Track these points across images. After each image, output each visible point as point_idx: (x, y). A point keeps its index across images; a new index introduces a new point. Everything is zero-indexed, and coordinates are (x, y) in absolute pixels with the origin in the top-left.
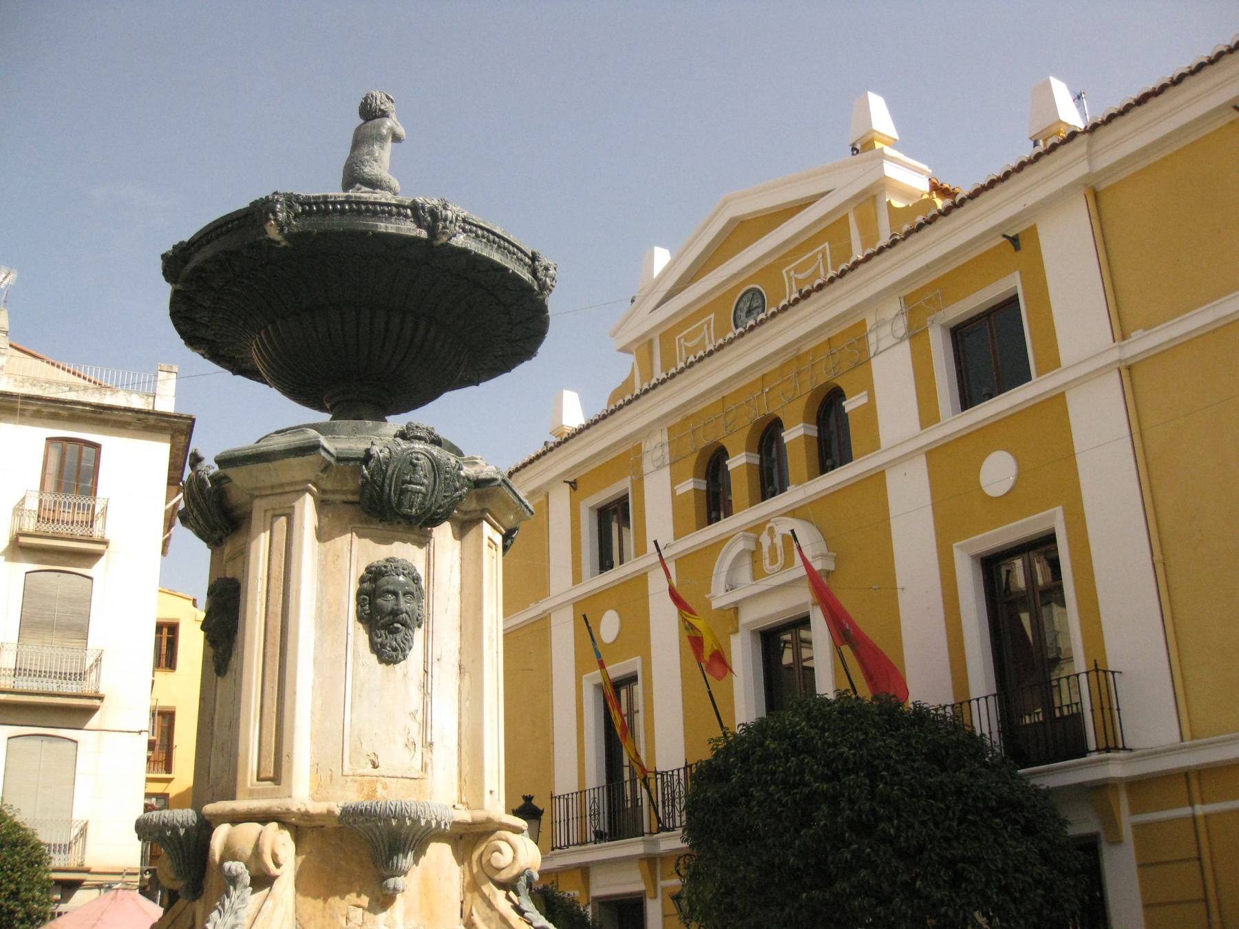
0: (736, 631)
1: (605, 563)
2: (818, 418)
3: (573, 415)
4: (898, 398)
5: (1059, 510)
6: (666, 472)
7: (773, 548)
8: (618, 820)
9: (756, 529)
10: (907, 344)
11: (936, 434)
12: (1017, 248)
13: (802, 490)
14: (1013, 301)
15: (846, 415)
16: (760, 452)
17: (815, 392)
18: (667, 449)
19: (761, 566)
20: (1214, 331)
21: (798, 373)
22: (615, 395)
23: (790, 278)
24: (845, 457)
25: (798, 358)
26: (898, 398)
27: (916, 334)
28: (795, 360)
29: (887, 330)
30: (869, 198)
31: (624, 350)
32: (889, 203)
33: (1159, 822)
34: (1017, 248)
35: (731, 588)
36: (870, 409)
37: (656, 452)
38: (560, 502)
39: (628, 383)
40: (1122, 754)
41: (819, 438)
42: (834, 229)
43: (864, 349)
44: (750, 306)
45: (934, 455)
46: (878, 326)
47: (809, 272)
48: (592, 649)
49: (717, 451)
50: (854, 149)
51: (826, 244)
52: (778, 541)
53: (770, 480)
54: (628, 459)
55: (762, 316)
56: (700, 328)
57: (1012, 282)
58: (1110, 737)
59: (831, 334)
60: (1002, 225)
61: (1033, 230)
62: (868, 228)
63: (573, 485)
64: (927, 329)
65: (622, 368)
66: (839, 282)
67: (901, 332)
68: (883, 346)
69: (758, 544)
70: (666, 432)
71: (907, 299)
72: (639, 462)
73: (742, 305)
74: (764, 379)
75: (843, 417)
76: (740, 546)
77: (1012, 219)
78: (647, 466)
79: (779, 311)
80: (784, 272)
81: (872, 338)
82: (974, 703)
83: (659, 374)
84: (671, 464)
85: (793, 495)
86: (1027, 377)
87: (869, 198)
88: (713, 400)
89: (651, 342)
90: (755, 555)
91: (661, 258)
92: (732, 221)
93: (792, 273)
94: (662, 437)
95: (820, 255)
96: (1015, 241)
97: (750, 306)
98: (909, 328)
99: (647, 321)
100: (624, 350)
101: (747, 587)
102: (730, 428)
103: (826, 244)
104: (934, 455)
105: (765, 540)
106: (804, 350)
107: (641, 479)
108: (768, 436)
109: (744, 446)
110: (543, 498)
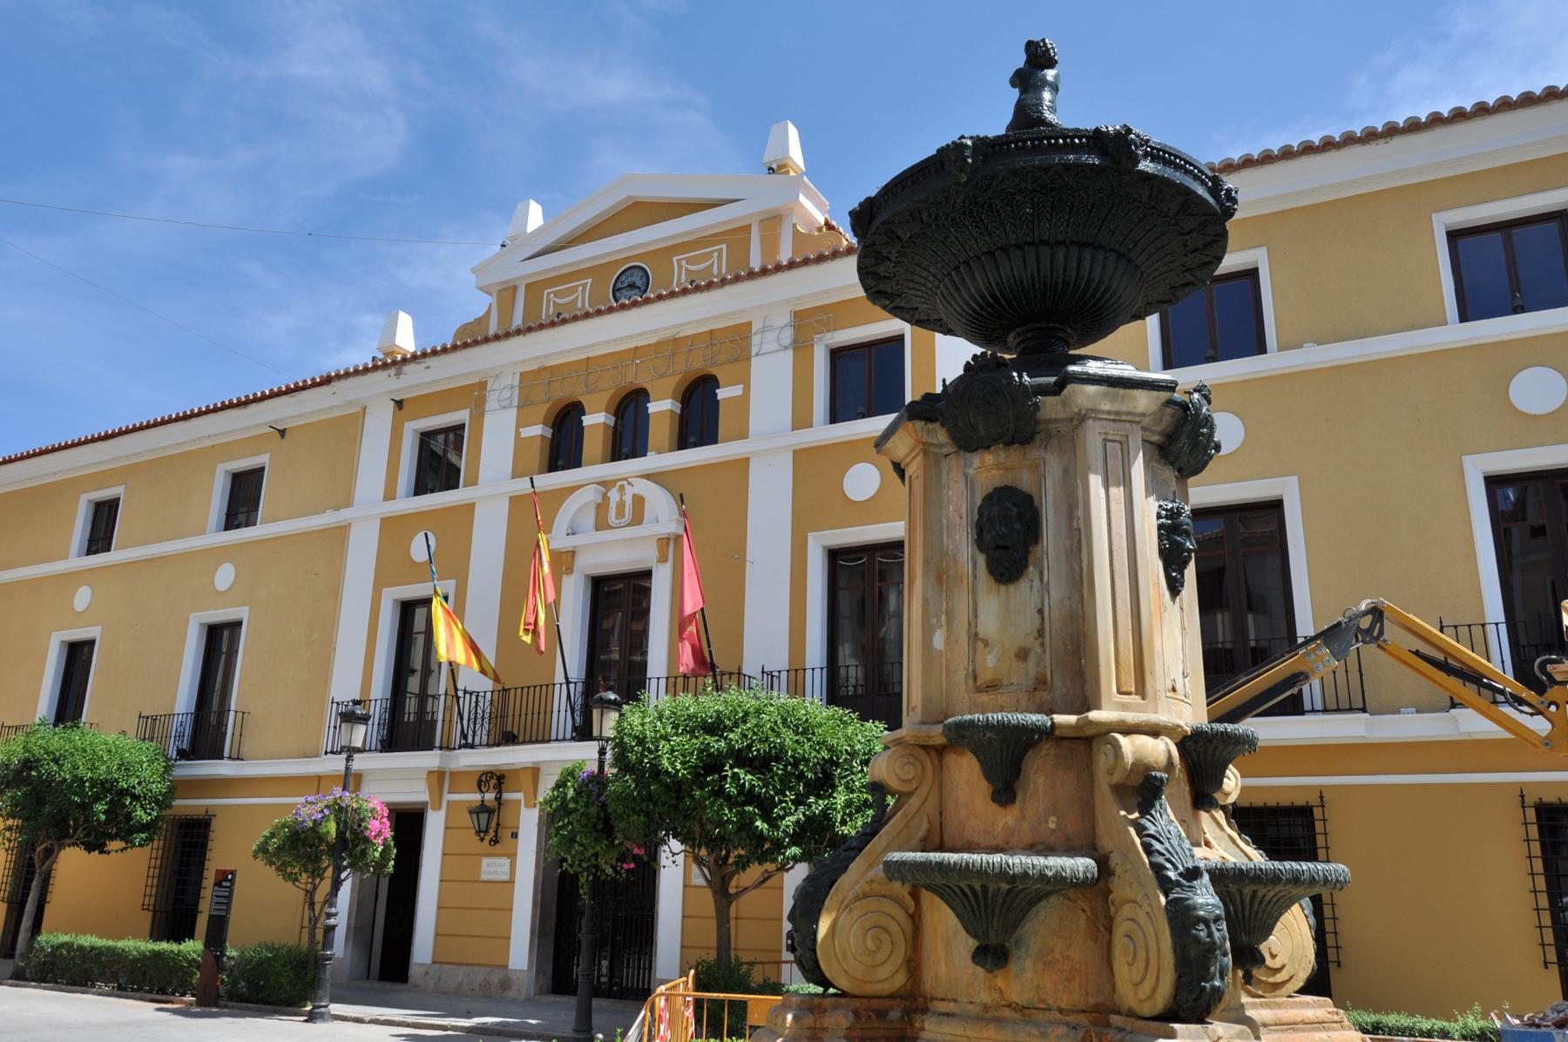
1: (231, 522)
2: (684, 396)
4: (773, 400)
6: (512, 413)
7: (621, 506)
8: (405, 730)
10: (790, 352)
11: (807, 438)
15: (717, 402)
16: (616, 415)
22: (463, 329)
23: (680, 267)
24: (708, 436)
27: (801, 345)
28: (672, 346)
29: (772, 336)
30: (772, 221)
35: (572, 533)
36: (743, 402)
39: (483, 320)
41: (682, 416)
42: (737, 237)
43: (748, 347)
44: (632, 286)
45: (802, 457)
46: (764, 330)
48: (391, 565)
51: (589, 281)
52: (628, 500)
53: (628, 438)
54: (474, 395)
56: (575, 289)
62: (770, 243)
63: (399, 404)
65: (477, 305)
69: (605, 498)
71: (797, 314)
74: (588, 366)
78: (492, 402)
81: (756, 340)
82: (809, 672)
85: (654, 461)
89: (515, 288)
90: (601, 507)
98: (795, 341)
103: (589, 281)
104: (802, 457)
105: (614, 495)
108: (630, 406)
109: (541, 418)
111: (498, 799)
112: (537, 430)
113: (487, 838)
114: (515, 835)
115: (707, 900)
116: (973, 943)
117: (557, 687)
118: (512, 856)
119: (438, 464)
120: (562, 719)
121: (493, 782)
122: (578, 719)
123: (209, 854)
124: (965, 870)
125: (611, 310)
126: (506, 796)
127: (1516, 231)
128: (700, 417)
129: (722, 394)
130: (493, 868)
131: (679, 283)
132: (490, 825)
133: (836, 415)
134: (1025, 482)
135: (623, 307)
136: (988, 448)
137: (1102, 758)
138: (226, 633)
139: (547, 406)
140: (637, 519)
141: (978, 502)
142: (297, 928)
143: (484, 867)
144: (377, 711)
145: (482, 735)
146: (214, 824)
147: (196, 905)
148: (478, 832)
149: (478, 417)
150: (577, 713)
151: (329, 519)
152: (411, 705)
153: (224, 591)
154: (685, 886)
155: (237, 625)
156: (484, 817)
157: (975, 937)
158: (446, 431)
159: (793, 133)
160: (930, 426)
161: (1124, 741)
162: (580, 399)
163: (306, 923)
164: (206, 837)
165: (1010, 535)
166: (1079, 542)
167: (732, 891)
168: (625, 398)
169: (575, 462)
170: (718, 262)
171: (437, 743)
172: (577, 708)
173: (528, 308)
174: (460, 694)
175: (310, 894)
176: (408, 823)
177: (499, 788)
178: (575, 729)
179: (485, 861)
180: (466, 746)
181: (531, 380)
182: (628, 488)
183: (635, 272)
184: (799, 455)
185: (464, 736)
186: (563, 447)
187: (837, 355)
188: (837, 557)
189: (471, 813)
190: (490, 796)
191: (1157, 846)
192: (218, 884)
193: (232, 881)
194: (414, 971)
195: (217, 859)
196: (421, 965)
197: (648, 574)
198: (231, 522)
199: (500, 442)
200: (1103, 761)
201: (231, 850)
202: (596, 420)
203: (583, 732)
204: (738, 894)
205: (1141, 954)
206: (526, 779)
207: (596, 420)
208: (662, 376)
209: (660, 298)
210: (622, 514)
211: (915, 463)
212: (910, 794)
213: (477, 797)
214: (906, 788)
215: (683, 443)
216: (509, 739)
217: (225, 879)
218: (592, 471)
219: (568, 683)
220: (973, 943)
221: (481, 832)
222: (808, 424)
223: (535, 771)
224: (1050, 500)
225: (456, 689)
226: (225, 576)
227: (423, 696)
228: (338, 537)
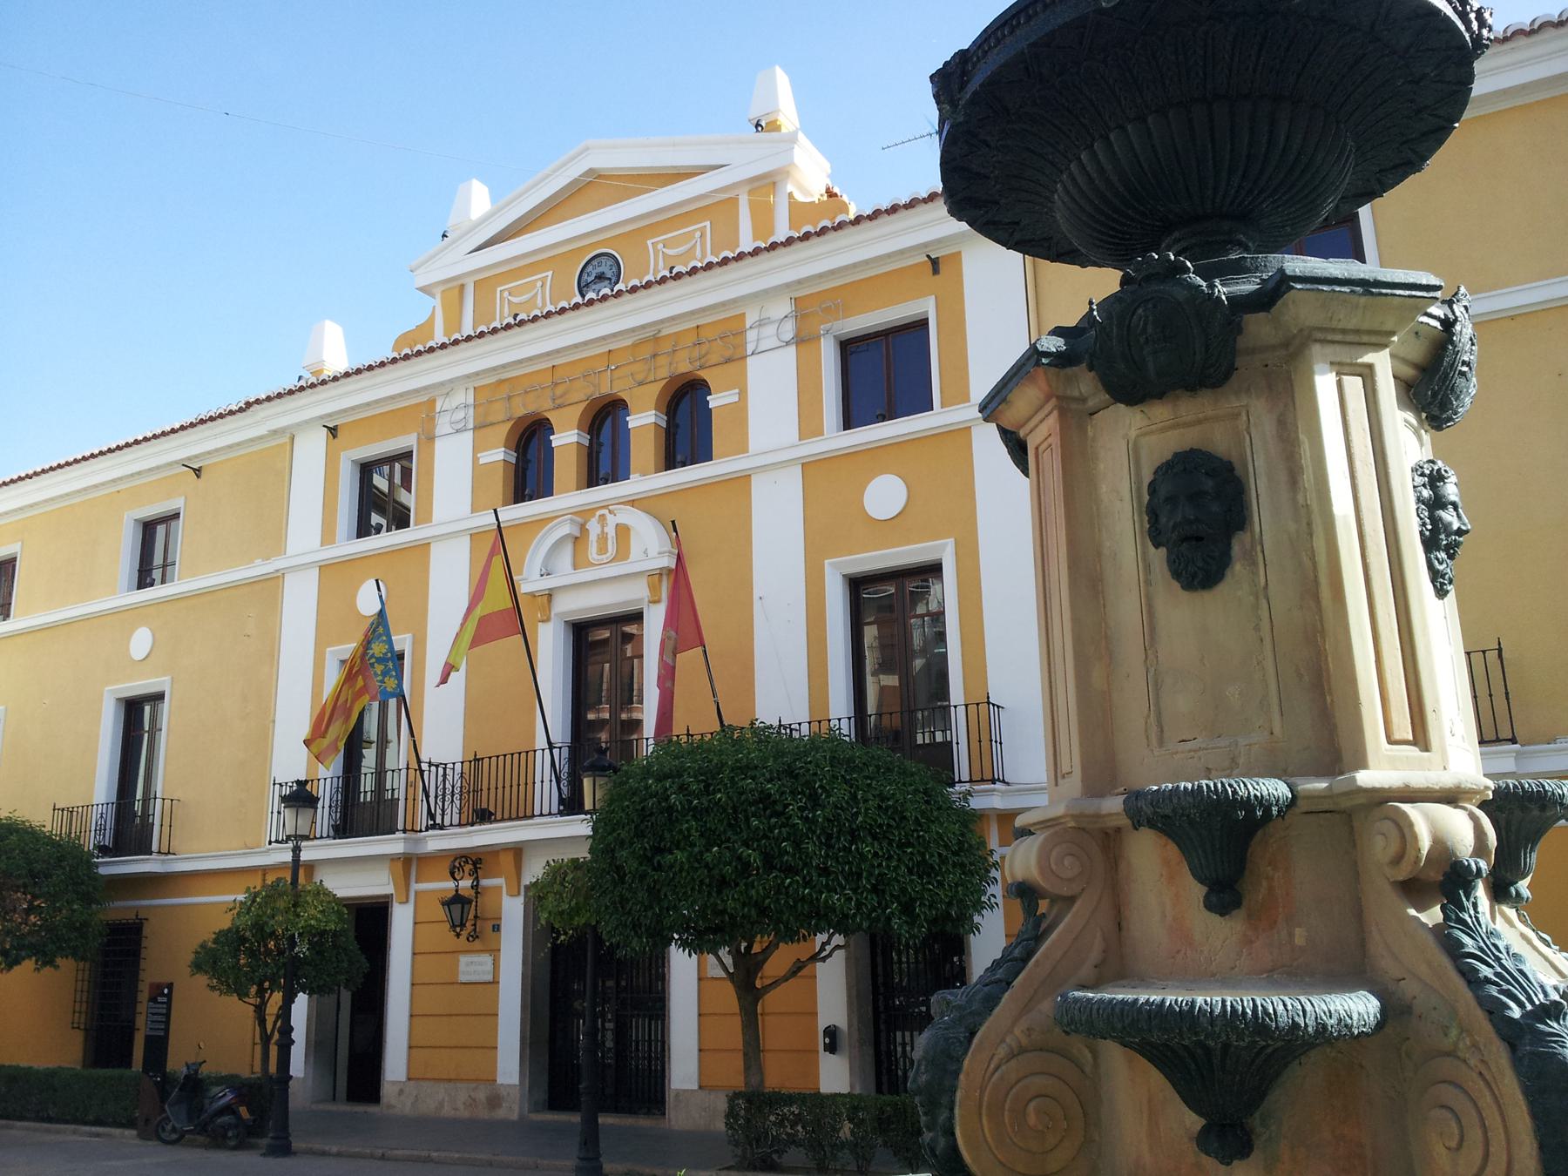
0: (548, 620)
1: (144, 579)
2: (669, 406)
3: (336, 360)
4: (775, 403)
5: (950, 543)
7: (603, 538)
8: (359, 814)
9: (584, 514)
10: (793, 349)
12: (936, 271)
13: (646, 481)
14: (923, 323)
17: (672, 379)
18: (471, 411)
19: (604, 547)
20: (1512, 318)
21: (655, 356)
23: (656, 252)
24: (702, 452)
25: (656, 339)
26: (775, 403)
27: (804, 339)
28: (651, 341)
29: (770, 330)
30: (766, 184)
31: (425, 290)
32: (790, 194)
33: (173, 906)
34: (936, 271)
36: (739, 411)
37: (455, 409)
38: (311, 452)
39: (426, 328)
40: (998, 786)
42: (720, 208)
44: (599, 276)
45: (810, 467)
46: (761, 323)
47: (682, 249)
49: (534, 423)
50: (758, 125)
51: (708, 224)
52: (610, 531)
53: (603, 464)
54: (421, 412)
55: (607, 291)
57: (926, 306)
58: (986, 764)
59: (701, 322)
60: (926, 245)
61: (956, 257)
63: (333, 431)
64: (819, 338)
65: (416, 311)
66: (657, 288)
67: (789, 336)
68: (763, 346)
69: (583, 527)
70: (471, 392)
72: (431, 420)
73: (590, 268)
74: (555, 373)
75: (704, 416)
76: (566, 529)
77: (939, 241)
78: (443, 425)
79: (835, 229)
80: (649, 242)
81: (751, 336)
83: (468, 330)
84: (475, 429)
86: (928, 406)
87: (766, 184)
88: (544, 366)
89: (462, 286)
90: (578, 540)
91: (478, 202)
92: (591, 171)
93: (660, 246)
94: (464, 397)
95: (698, 234)
96: (935, 264)
97: (599, 276)
99: (459, 262)
100: (425, 290)
101: (565, 574)
102: (558, 402)
104: (325, 568)
105: (594, 527)
106: (664, 333)
107: (431, 439)
108: (605, 417)
110: (286, 439)
111: (475, 887)
112: (497, 454)
113: (464, 934)
114: (497, 928)
115: (728, 997)
116: (1194, 1122)
117: (539, 753)
118: (495, 952)
119: (381, 499)
120: (546, 792)
121: (468, 868)
122: (565, 790)
123: (143, 964)
124: (1188, 1017)
125: (577, 306)
126: (484, 882)
127: (520, 637)
128: (688, 426)
129: (714, 401)
130: (472, 967)
131: (656, 271)
132: (466, 917)
133: (848, 423)
134: (1219, 441)
135: (591, 302)
136: (1160, 396)
137: (1379, 841)
138: (147, 709)
139: (509, 425)
140: (622, 553)
141: (1147, 477)
142: (250, 1042)
143: (462, 967)
144: (325, 792)
145: (453, 815)
146: (146, 930)
147: (133, 1021)
148: (453, 926)
149: (429, 438)
150: (564, 783)
151: (260, 568)
152: (367, 784)
153: (140, 658)
154: (700, 979)
155: (158, 697)
156: (457, 908)
157: (1200, 1113)
158: (390, 460)
159: (782, 80)
160: (1069, 371)
161: (1414, 812)
162: (548, 415)
163: (258, 1040)
164: (138, 943)
165: (1202, 520)
166: (1309, 524)
167: (758, 984)
168: (605, 407)
169: (544, 489)
170: (699, 244)
171: (400, 826)
172: (564, 776)
173: (476, 307)
174: (425, 767)
175: (260, 1010)
176: (370, 919)
177: (475, 873)
178: (561, 801)
179: (464, 959)
180: (434, 827)
181: (491, 389)
182: (609, 517)
183: (604, 260)
184: (810, 467)
185: (431, 816)
186: (528, 472)
187: (848, 347)
188: (857, 585)
189: (443, 904)
190: (466, 884)
191: (1486, 971)
192: (153, 999)
193: (169, 996)
194: (387, 1091)
195: (152, 971)
196: (394, 1083)
197: (637, 617)
198: (144, 579)
199: (456, 477)
200: (1380, 847)
201: (169, 956)
202: (566, 438)
203: (571, 805)
204: (768, 988)
205: (1475, 1135)
206: (507, 860)
207: (566, 438)
208: (641, 384)
209: (634, 290)
210: (604, 547)
211: (1043, 431)
212: (1071, 900)
213: (451, 884)
214: (1065, 891)
215: (670, 460)
216: (483, 816)
217: (163, 994)
218: (567, 499)
219: (551, 746)
220: (1194, 1122)
221: (457, 926)
222: (819, 432)
223: (518, 851)
224: (1260, 462)
225: (419, 762)
226: (141, 642)
227: (380, 772)
228: (271, 586)
